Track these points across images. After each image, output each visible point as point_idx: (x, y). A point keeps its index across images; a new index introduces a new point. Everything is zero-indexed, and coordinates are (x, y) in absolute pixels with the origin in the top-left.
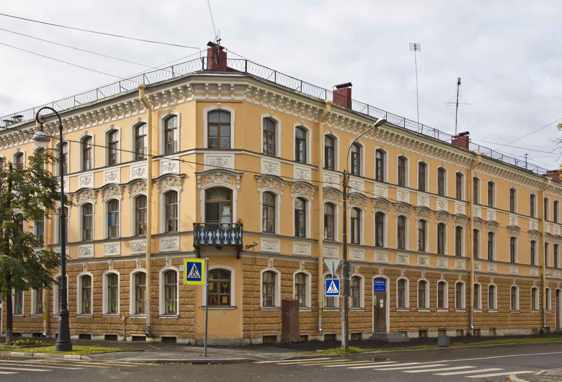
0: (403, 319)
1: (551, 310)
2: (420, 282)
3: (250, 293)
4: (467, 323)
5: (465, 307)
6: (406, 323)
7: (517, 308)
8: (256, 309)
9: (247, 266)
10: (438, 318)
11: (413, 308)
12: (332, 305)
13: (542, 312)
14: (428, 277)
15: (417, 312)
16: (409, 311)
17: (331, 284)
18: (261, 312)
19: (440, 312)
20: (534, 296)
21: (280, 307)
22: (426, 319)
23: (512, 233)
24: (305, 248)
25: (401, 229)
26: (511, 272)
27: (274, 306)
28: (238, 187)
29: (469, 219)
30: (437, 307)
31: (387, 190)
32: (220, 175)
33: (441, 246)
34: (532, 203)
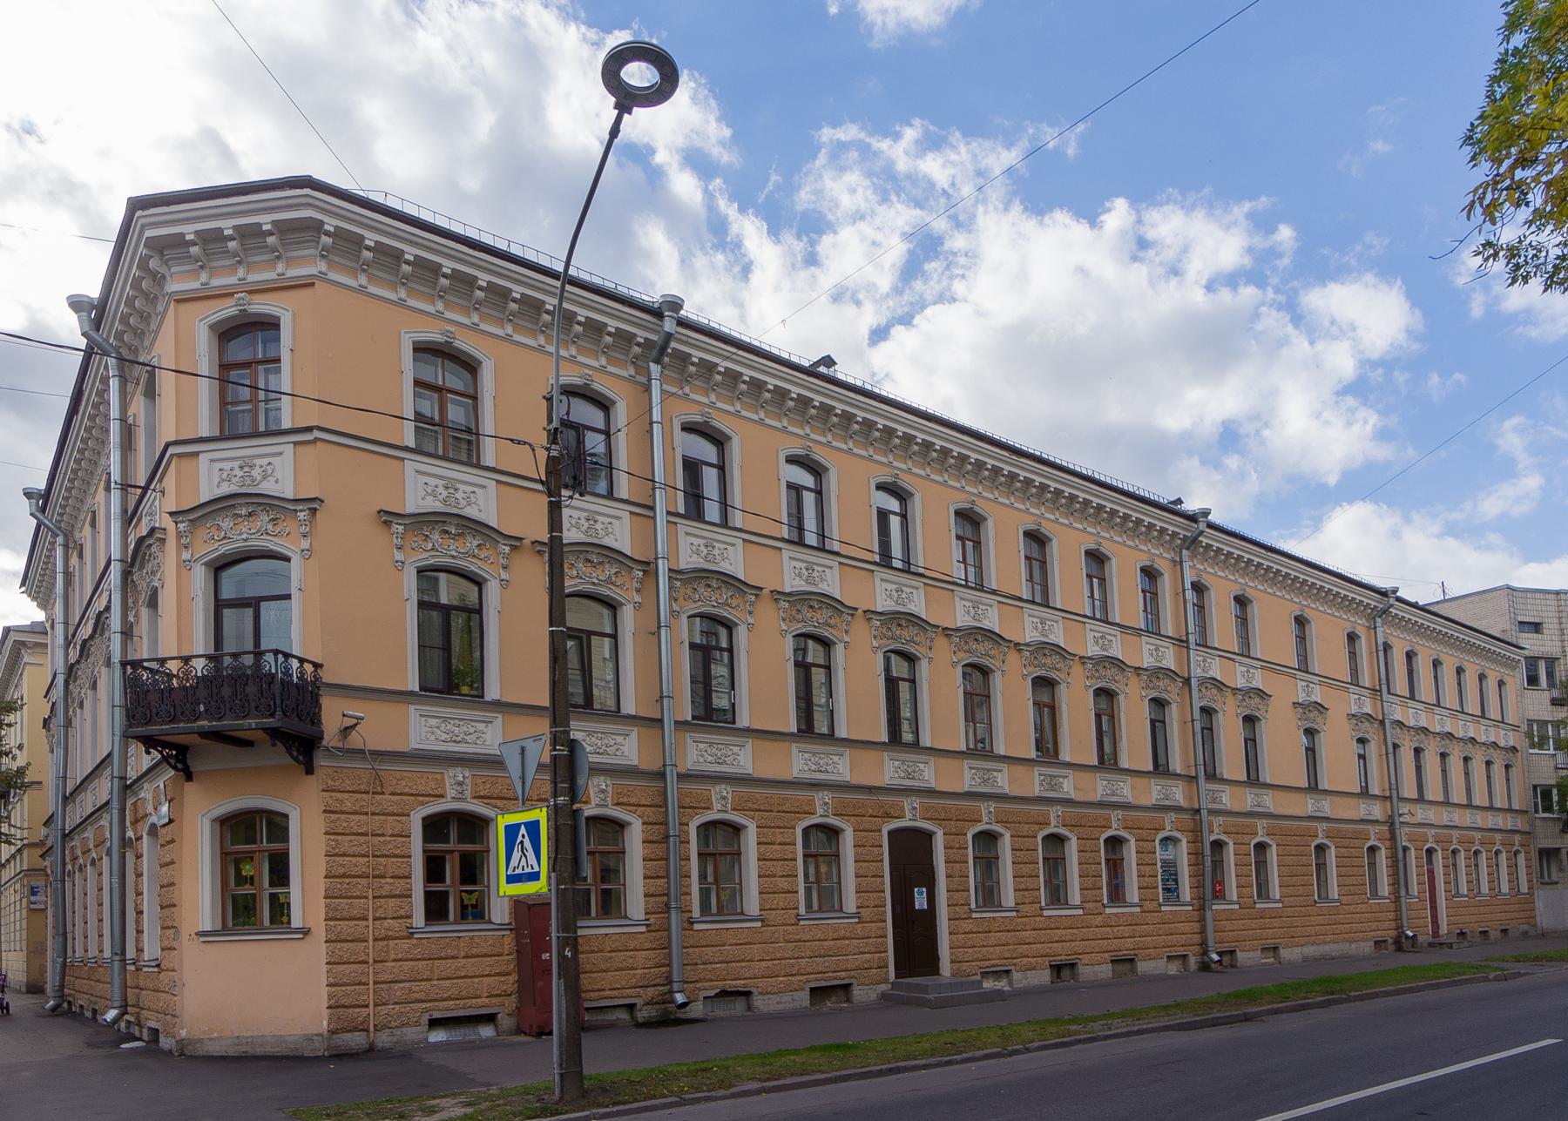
0: (994, 938)
1: (1416, 894)
2: (977, 836)
3: (364, 881)
4: (1197, 938)
5: (1188, 899)
6: (1007, 948)
7: (1333, 893)
8: (390, 933)
9: (346, 796)
10: (1108, 929)
11: (1026, 908)
12: (739, 911)
13: (1397, 900)
14: (1072, 826)
15: (1041, 916)
16: (1014, 914)
17: (520, 839)
18: (414, 942)
19: (1115, 914)
20: (1372, 865)
21: (510, 924)
22: (1071, 934)
23: (1359, 730)
24: (831, 762)
25: (1158, 726)
26: (1310, 809)
27: (490, 922)
28: (305, 544)
29: (1187, 681)
30: (1105, 902)
31: (922, 591)
32: (250, 514)
33: (1252, 764)
34: (1353, 655)
